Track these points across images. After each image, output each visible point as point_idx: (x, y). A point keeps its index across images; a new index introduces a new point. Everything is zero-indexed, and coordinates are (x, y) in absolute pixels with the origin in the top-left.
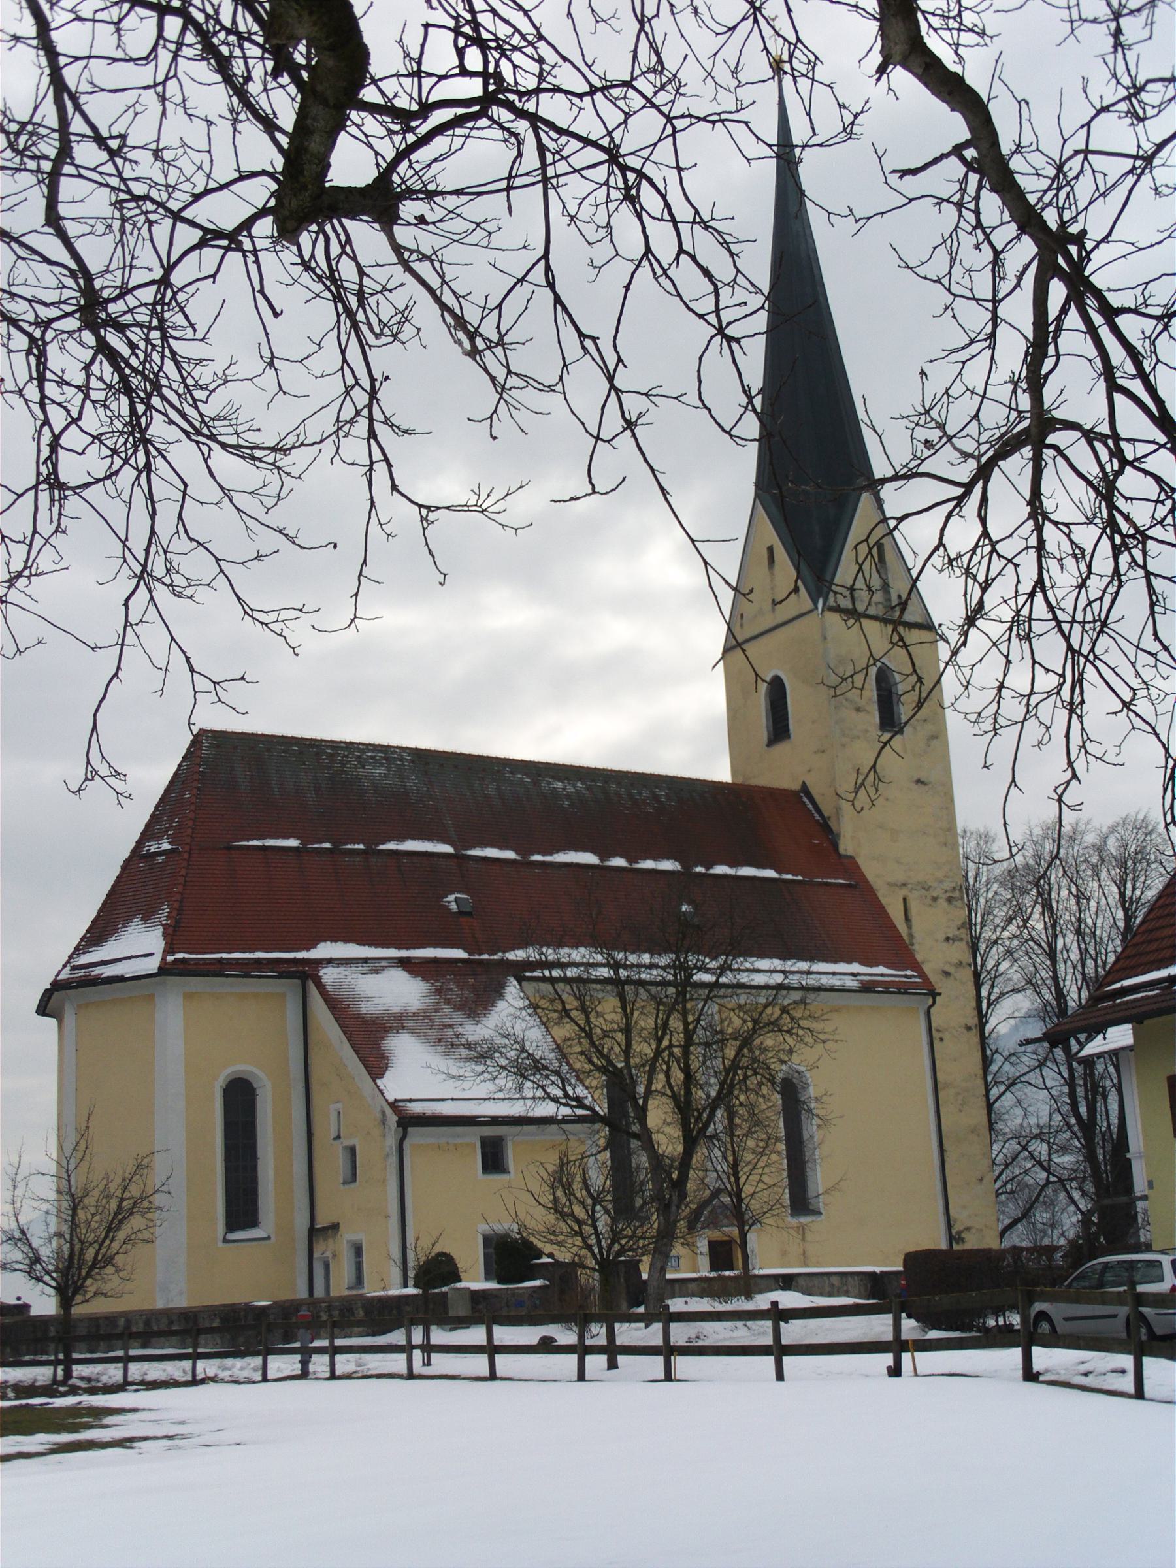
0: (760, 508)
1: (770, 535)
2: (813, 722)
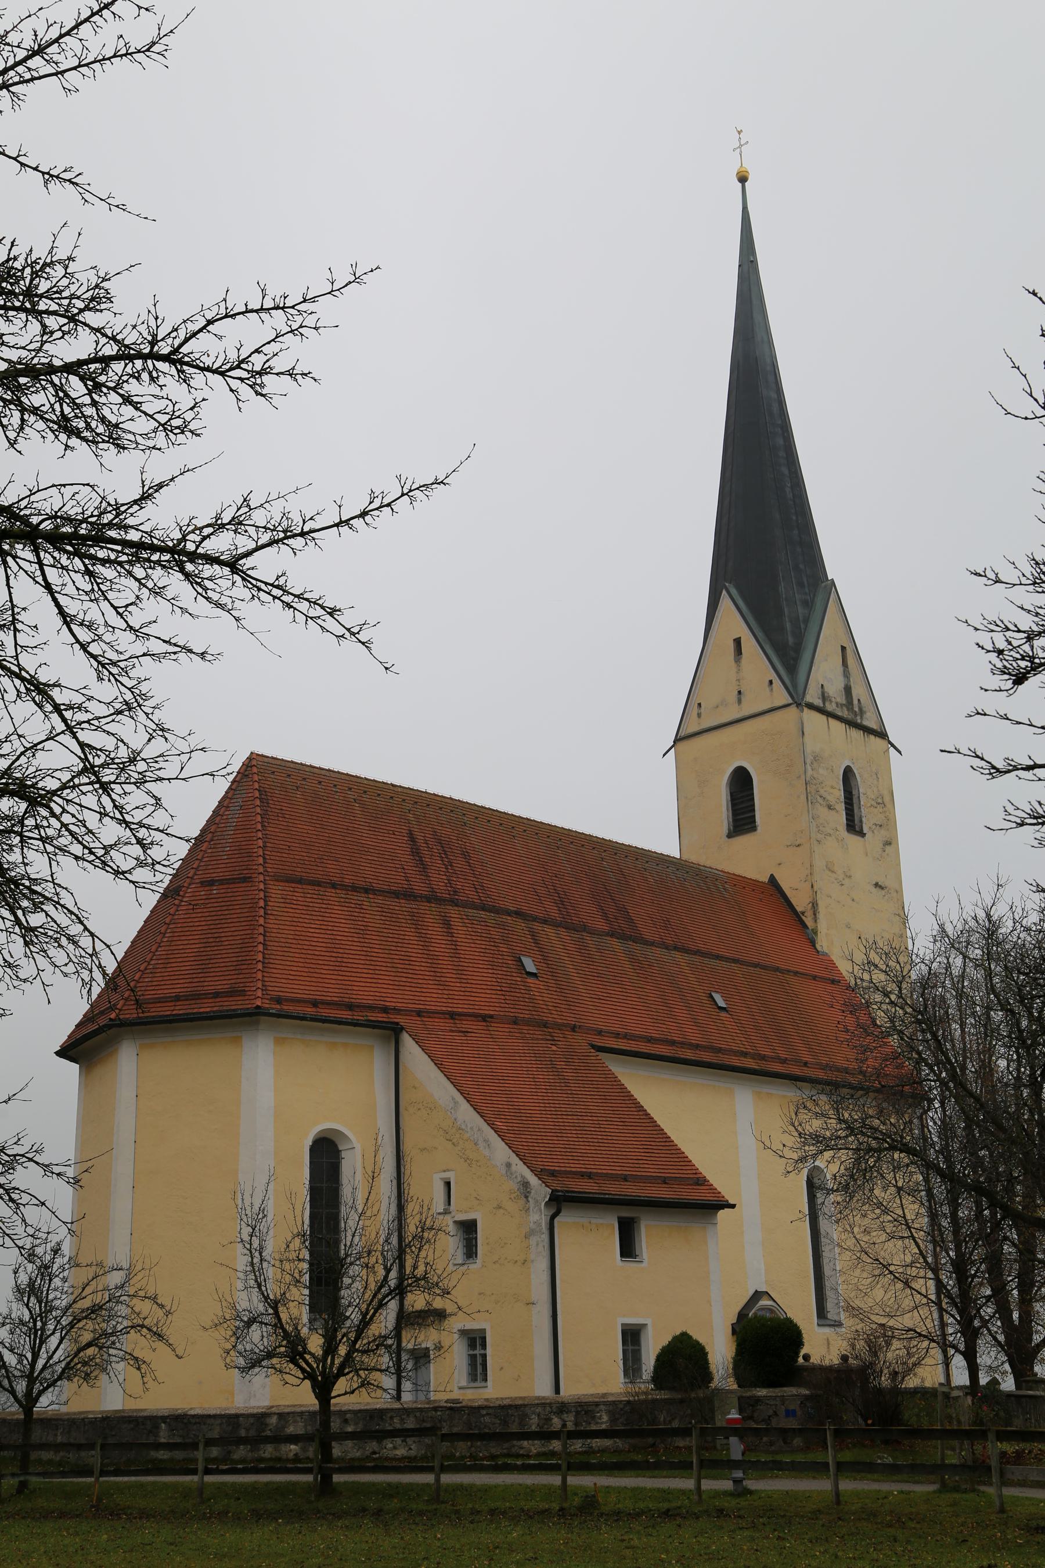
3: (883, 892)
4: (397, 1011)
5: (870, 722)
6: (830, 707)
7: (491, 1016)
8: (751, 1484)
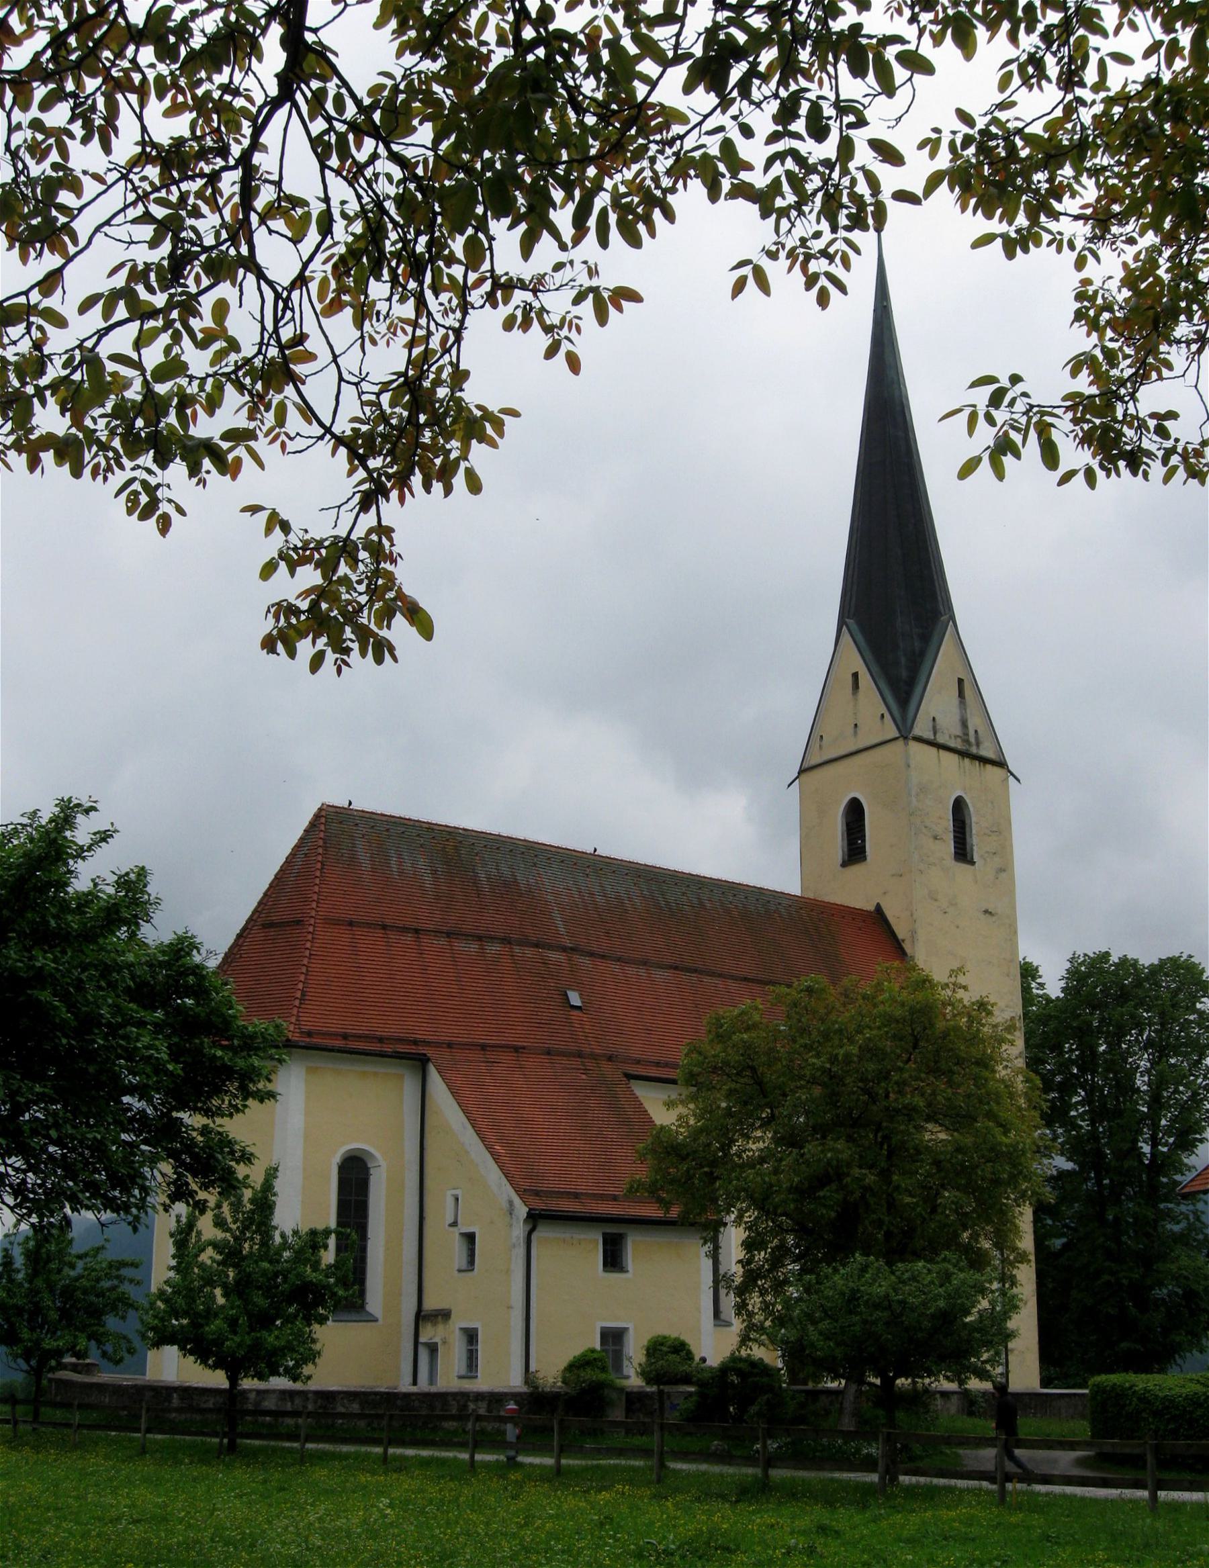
0: (846, 637)
1: (854, 661)
2: (892, 846)
3: (994, 919)
4: (427, 1043)
5: (987, 751)
6: (941, 739)
7: (524, 1048)
8: (520, 1459)
